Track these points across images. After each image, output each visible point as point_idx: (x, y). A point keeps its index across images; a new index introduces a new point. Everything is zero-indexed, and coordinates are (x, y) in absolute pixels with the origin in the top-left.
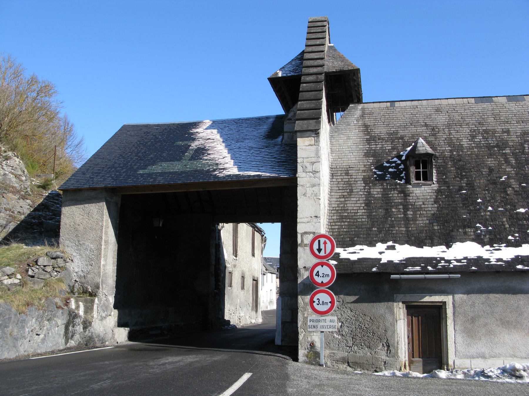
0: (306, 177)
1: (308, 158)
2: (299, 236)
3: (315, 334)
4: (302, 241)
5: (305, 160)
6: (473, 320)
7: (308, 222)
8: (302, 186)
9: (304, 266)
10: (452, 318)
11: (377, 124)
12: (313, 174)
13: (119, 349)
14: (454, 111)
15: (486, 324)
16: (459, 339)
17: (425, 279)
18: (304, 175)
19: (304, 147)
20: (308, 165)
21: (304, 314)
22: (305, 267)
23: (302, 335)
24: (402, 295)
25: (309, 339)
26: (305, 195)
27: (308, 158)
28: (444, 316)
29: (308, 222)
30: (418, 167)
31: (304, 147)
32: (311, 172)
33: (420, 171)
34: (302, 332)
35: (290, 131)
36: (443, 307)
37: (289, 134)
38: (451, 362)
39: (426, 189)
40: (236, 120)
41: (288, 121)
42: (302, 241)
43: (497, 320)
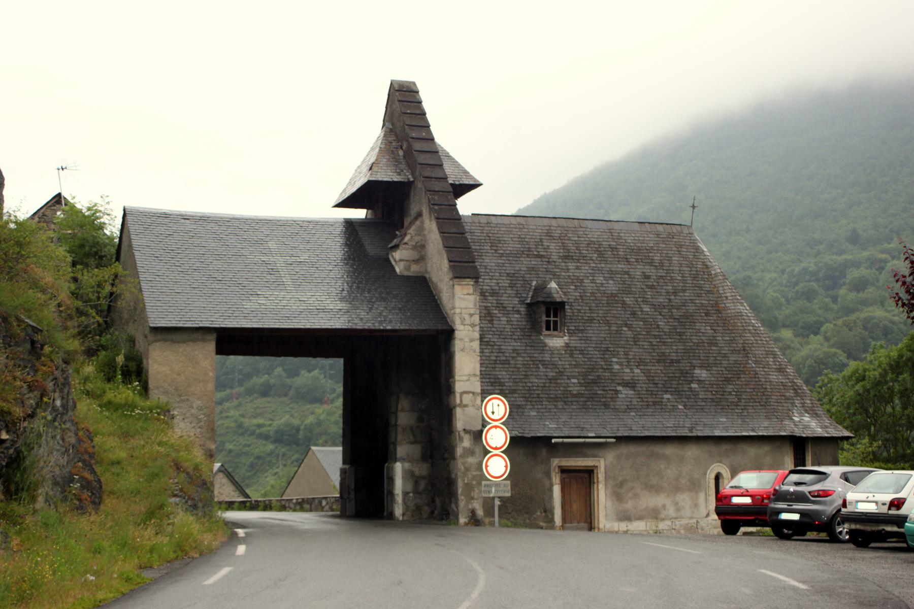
0: (464, 330)
1: (467, 308)
2: (458, 396)
3: (475, 501)
4: (461, 401)
5: (464, 311)
6: (621, 485)
7: (467, 381)
8: (461, 340)
9: (463, 428)
10: (603, 482)
11: (482, 248)
12: (472, 327)
13: (399, 499)
14: (566, 238)
15: (632, 488)
16: (609, 504)
17: (563, 444)
18: (461, 327)
19: (462, 296)
20: (467, 317)
21: (464, 480)
22: (464, 430)
23: (463, 502)
24: (558, 459)
25: (470, 507)
26: (462, 350)
27: (467, 308)
28: (595, 480)
29: (467, 381)
30: (548, 315)
31: (462, 296)
32: (470, 325)
33: (550, 317)
34: (463, 500)
35: (407, 259)
36: (595, 471)
37: (405, 262)
38: (601, 526)
39: (558, 341)
40: (300, 221)
41: (404, 246)
42: (461, 401)
43: (642, 483)
